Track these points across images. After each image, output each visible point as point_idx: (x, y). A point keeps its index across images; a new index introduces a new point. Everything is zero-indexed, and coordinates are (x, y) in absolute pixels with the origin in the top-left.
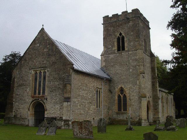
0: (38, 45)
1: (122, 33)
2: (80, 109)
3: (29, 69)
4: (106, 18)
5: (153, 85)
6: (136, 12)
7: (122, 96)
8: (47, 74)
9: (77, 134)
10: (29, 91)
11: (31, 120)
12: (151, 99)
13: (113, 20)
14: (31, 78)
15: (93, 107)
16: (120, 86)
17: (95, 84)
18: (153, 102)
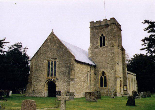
0: (50, 43)
1: (103, 34)
2: (79, 85)
3: (44, 59)
4: (92, 23)
5: (124, 69)
6: (113, 19)
7: (103, 77)
8: (57, 63)
9: (88, 99)
10: (44, 73)
11: (45, 93)
12: (122, 79)
13: (97, 25)
14: (46, 66)
15: (86, 84)
16: (102, 70)
17: (87, 69)
18: (123, 81)
